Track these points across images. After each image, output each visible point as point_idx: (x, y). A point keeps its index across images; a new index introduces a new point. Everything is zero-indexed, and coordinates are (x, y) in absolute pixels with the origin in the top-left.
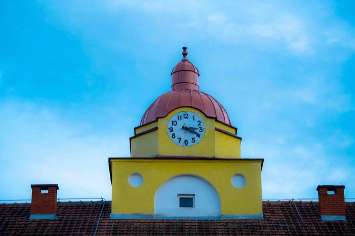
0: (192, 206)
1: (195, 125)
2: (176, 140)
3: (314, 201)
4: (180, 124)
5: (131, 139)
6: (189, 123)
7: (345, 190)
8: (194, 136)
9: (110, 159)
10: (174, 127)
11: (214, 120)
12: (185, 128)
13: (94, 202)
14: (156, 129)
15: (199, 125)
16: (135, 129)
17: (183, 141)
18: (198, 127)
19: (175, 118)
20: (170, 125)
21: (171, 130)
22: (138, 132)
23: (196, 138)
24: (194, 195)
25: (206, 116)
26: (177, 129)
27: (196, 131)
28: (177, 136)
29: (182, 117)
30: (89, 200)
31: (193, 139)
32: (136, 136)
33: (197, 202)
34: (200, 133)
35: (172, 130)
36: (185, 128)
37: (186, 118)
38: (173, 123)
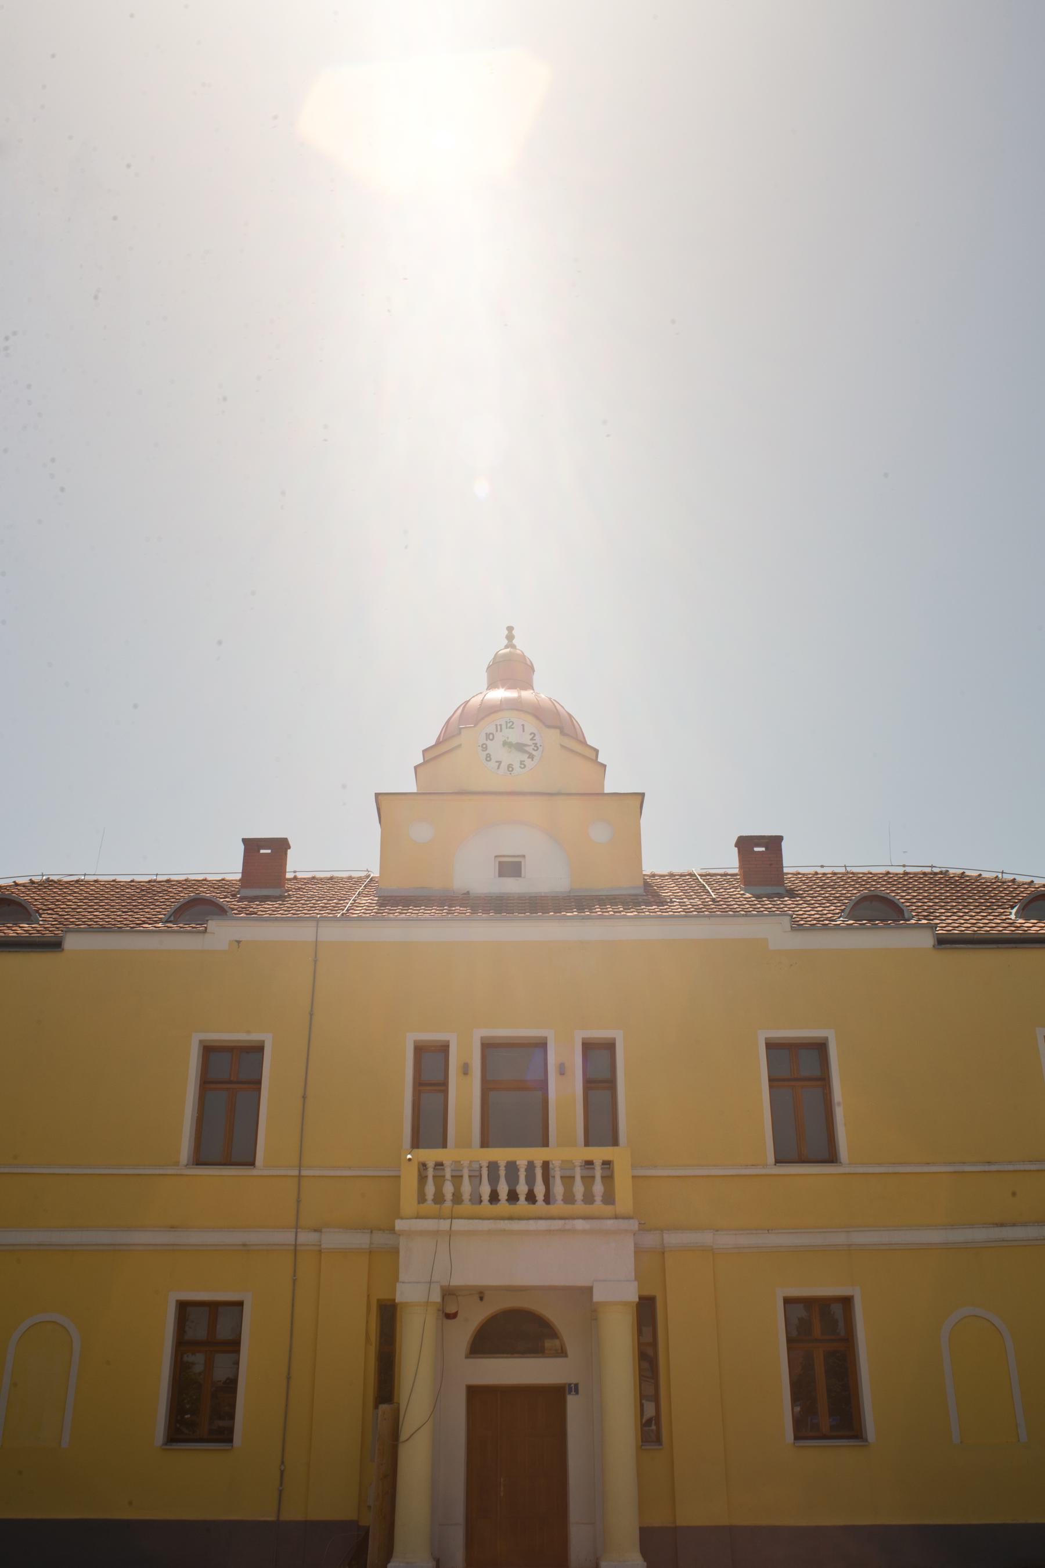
0: (520, 876)
1: (526, 739)
2: (493, 764)
3: (229, 877)
4: (500, 737)
5: (416, 768)
6: (514, 736)
7: (783, 843)
8: (525, 757)
9: (377, 795)
10: (488, 742)
11: (558, 731)
12: (505, 744)
13: (875, 875)
14: (459, 746)
15: (532, 739)
16: (424, 751)
17: (504, 765)
18: (530, 743)
19: (491, 729)
20: (482, 740)
21: (485, 748)
22: (429, 756)
23: (528, 762)
24: (524, 856)
25: (544, 723)
26: (496, 749)
27: (527, 748)
28: (494, 759)
29: (504, 727)
30: (865, 870)
31: (522, 762)
32: (425, 762)
33: (527, 869)
34: (534, 753)
35: (486, 748)
36: (505, 744)
37: (511, 728)
38: (487, 735)
